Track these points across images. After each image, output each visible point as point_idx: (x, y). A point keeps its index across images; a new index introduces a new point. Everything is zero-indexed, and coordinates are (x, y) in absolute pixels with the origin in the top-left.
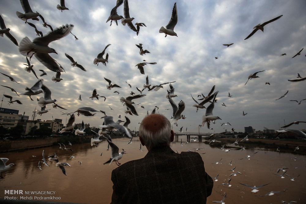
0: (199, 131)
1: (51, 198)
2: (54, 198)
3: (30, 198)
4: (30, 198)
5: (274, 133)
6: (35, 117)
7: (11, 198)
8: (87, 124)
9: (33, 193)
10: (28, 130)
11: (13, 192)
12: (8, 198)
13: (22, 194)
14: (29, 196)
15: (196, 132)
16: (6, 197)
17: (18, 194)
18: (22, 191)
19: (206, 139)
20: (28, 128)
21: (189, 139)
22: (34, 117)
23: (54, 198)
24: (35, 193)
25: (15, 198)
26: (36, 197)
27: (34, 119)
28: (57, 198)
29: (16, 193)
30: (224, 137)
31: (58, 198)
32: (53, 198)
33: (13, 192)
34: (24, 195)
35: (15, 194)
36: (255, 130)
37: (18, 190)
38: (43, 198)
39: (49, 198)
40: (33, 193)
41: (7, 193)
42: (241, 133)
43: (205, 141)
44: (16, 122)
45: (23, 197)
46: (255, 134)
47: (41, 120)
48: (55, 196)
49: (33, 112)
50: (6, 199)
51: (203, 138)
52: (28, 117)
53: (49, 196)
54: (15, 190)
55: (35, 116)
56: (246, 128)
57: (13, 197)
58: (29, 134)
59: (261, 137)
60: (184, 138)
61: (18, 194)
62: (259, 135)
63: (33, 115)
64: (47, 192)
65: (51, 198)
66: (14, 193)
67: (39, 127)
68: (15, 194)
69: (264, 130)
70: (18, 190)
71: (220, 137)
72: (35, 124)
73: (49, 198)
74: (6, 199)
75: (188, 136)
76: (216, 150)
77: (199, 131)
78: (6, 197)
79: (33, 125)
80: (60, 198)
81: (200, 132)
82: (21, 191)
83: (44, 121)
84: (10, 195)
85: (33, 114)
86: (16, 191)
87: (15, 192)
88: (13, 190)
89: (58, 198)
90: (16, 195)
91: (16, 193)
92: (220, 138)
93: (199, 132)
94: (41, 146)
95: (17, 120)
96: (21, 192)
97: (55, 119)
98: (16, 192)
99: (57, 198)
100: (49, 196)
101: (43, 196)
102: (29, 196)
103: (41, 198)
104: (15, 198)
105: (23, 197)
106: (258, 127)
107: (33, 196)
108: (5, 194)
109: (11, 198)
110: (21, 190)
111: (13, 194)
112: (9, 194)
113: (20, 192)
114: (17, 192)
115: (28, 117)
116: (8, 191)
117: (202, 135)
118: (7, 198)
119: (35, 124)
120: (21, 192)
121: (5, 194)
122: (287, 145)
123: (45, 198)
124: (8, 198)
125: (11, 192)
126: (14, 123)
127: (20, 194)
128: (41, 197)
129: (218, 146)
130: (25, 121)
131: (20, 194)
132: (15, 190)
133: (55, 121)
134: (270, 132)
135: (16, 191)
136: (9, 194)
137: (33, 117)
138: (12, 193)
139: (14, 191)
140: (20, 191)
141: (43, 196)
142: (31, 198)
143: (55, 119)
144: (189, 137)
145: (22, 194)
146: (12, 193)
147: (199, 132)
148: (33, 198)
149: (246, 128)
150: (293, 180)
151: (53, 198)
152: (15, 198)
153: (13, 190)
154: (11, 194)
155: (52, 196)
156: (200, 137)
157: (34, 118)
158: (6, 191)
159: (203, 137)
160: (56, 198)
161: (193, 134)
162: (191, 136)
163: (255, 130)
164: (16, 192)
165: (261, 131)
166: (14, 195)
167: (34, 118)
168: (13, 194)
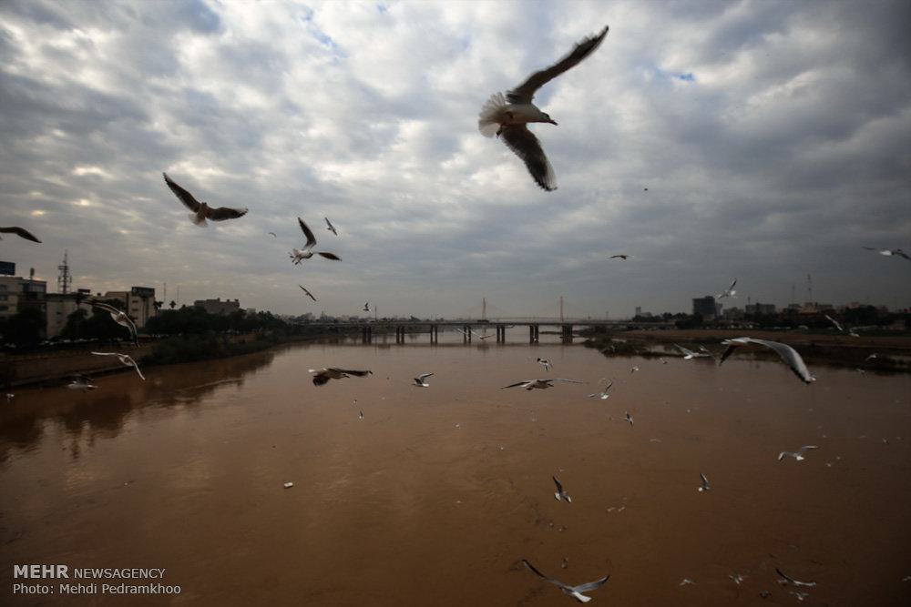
0: (562, 313)
1: (152, 590)
2: (162, 589)
3: (90, 590)
4: (90, 590)
5: (777, 315)
6: (68, 284)
7: (32, 590)
8: (232, 300)
9: (97, 573)
10: (54, 325)
11: (38, 571)
12: (24, 589)
13: (66, 576)
14: (85, 582)
15: (554, 315)
16: (17, 587)
17: (52, 576)
18: (66, 568)
19: (582, 333)
20: (54, 321)
21: (537, 337)
22: (65, 282)
23: (162, 589)
24: (104, 574)
25: (45, 590)
26: (106, 587)
27: (68, 289)
28: (169, 590)
29: (48, 574)
30: (637, 328)
31: (173, 590)
32: (157, 590)
33: (38, 571)
34: (73, 581)
35: (44, 576)
36: (721, 305)
37: (52, 567)
38: (129, 589)
39: (146, 589)
40: (97, 573)
41: (21, 574)
42: (683, 316)
43: (582, 339)
44: (14, 300)
45: (68, 586)
46: (721, 317)
47: (89, 291)
48: (165, 581)
49: (60, 268)
50: (19, 591)
51: (576, 332)
52: (43, 285)
53: (147, 582)
54: (44, 567)
55: (68, 279)
56: (697, 302)
57: (38, 586)
58: (65, 334)
59: (740, 327)
60: (522, 334)
61: (52, 576)
62: (734, 320)
63: (62, 279)
64: (138, 571)
65: (152, 590)
66: (40, 574)
67: (90, 314)
68: (44, 576)
69: (747, 307)
70: (52, 567)
71: (625, 327)
72: (78, 303)
73: (146, 589)
74: (19, 591)
75: (534, 328)
76: (620, 362)
77: (562, 313)
78: (17, 587)
79: (71, 307)
80: (177, 590)
81: (565, 316)
82: (62, 569)
83: (99, 294)
84: (29, 582)
85: (60, 273)
86: (48, 568)
87: (45, 571)
88: (39, 566)
89: (173, 590)
90: (47, 581)
91: (48, 574)
92: (624, 330)
93: (562, 316)
94: (107, 369)
95: (13, 294)
96: (62, 571)
97: (133, 288)
98: (49, 571)
99: (169, 590)
100: (147, 582)
101: (129, 582)
102: (85, 582)
103: (123, 589)
104: (46, 590)
105: (68, 586)
106: (732, 299)
107: (99, 582)
108: (16, 576)
109: (32, 590)
110: (62, 566)
111: (39, 577)
112: (26, 576)
113: (59, 572)
114: (52, 571)
115: (43, 285)
116: (25, 567)
117: (573, 324)
118: (20, 589)
119: (78, 303)
120: (64, 573)
121: (16, 576)
122: (813, 346)
123: (135, 590)
124: (24, 589)
125: (33, 571)
126: (5, 302)
127: (59, 576)
128: (123, 587)
129: (626, 351)
130: (40, 296)
131: (59, 576)
132: (44, 567)
133: (132, 292)
134: (764, 312)
135: (48, 568)
136: (26, 576)
137: (62, 284)
138: (36, 574)
139: (41, 569)
140: (59, 567)
141: (129, 582)
142: (93, 589)
143: (133, 288)
144: (537, 329)
145: (66, 576)
146: (36, 574)
147: (562, 316)
148: (100, 589)
149: (697, 302)
150: (829, 465)
151: (157, 590)
152: (45, 590)
153: (39, 566)
154: (33, 576)
155: (155, 582)
156: (567, 331)
157: (65, 287)
158: (17, 568)
159: (575, 328)
160: (165, 590)
161: (546, 321)
162: (541, 329)
163: (721, 305)
164: (49, 571)
165: (739, 308)
166: (41, 582)
167: (65, 287)
168: (39, 577)
